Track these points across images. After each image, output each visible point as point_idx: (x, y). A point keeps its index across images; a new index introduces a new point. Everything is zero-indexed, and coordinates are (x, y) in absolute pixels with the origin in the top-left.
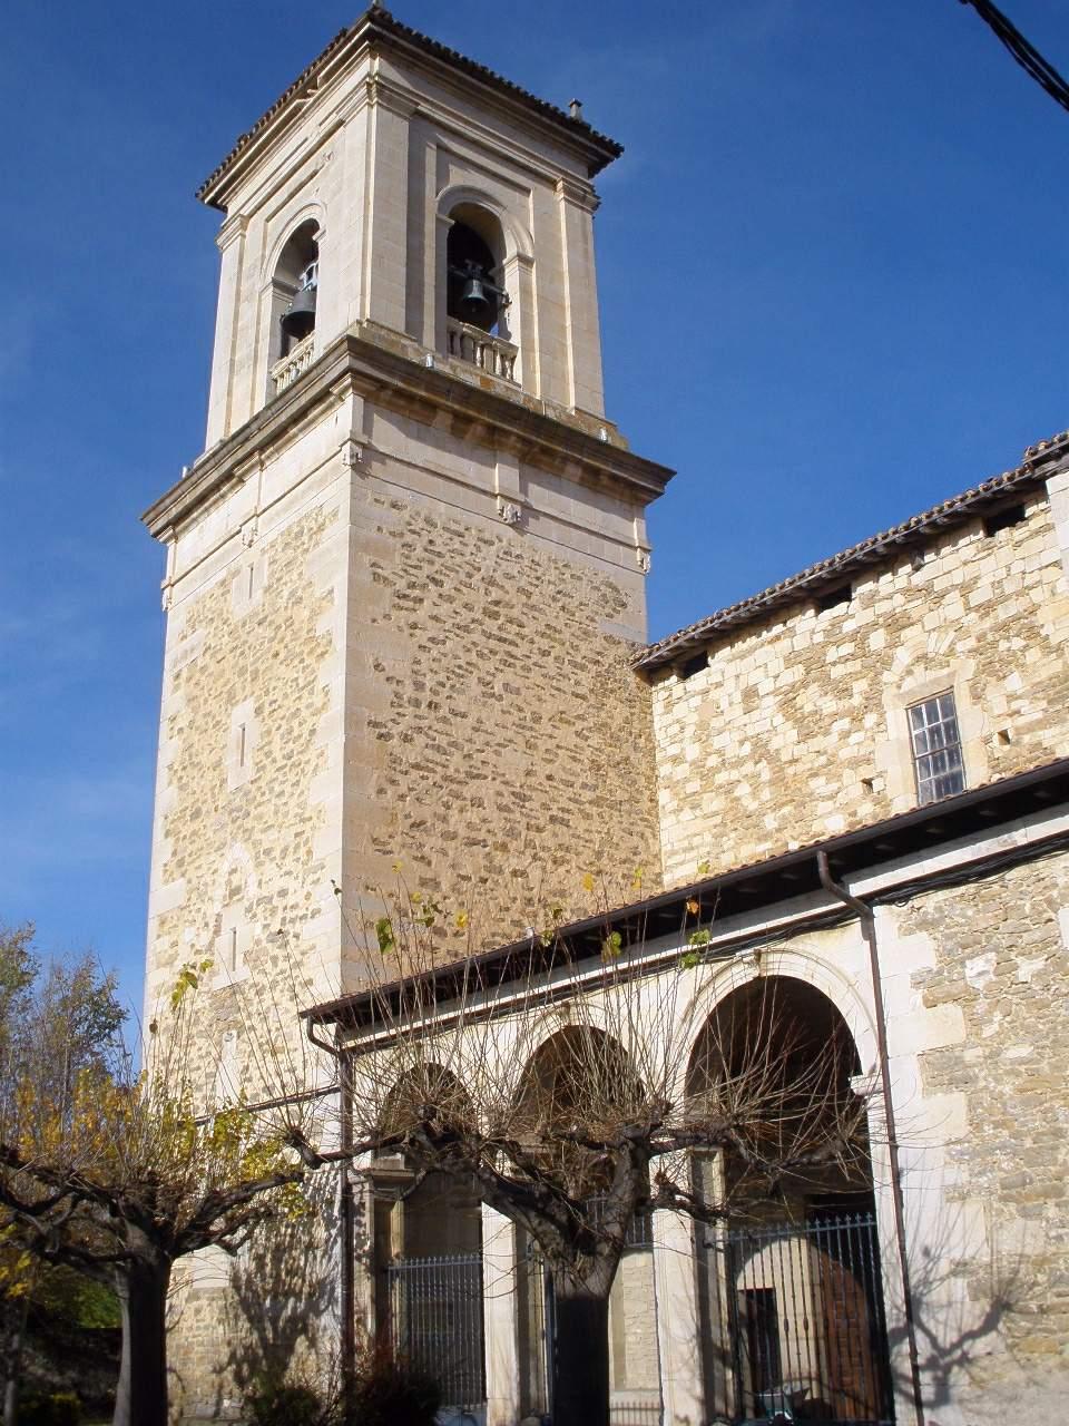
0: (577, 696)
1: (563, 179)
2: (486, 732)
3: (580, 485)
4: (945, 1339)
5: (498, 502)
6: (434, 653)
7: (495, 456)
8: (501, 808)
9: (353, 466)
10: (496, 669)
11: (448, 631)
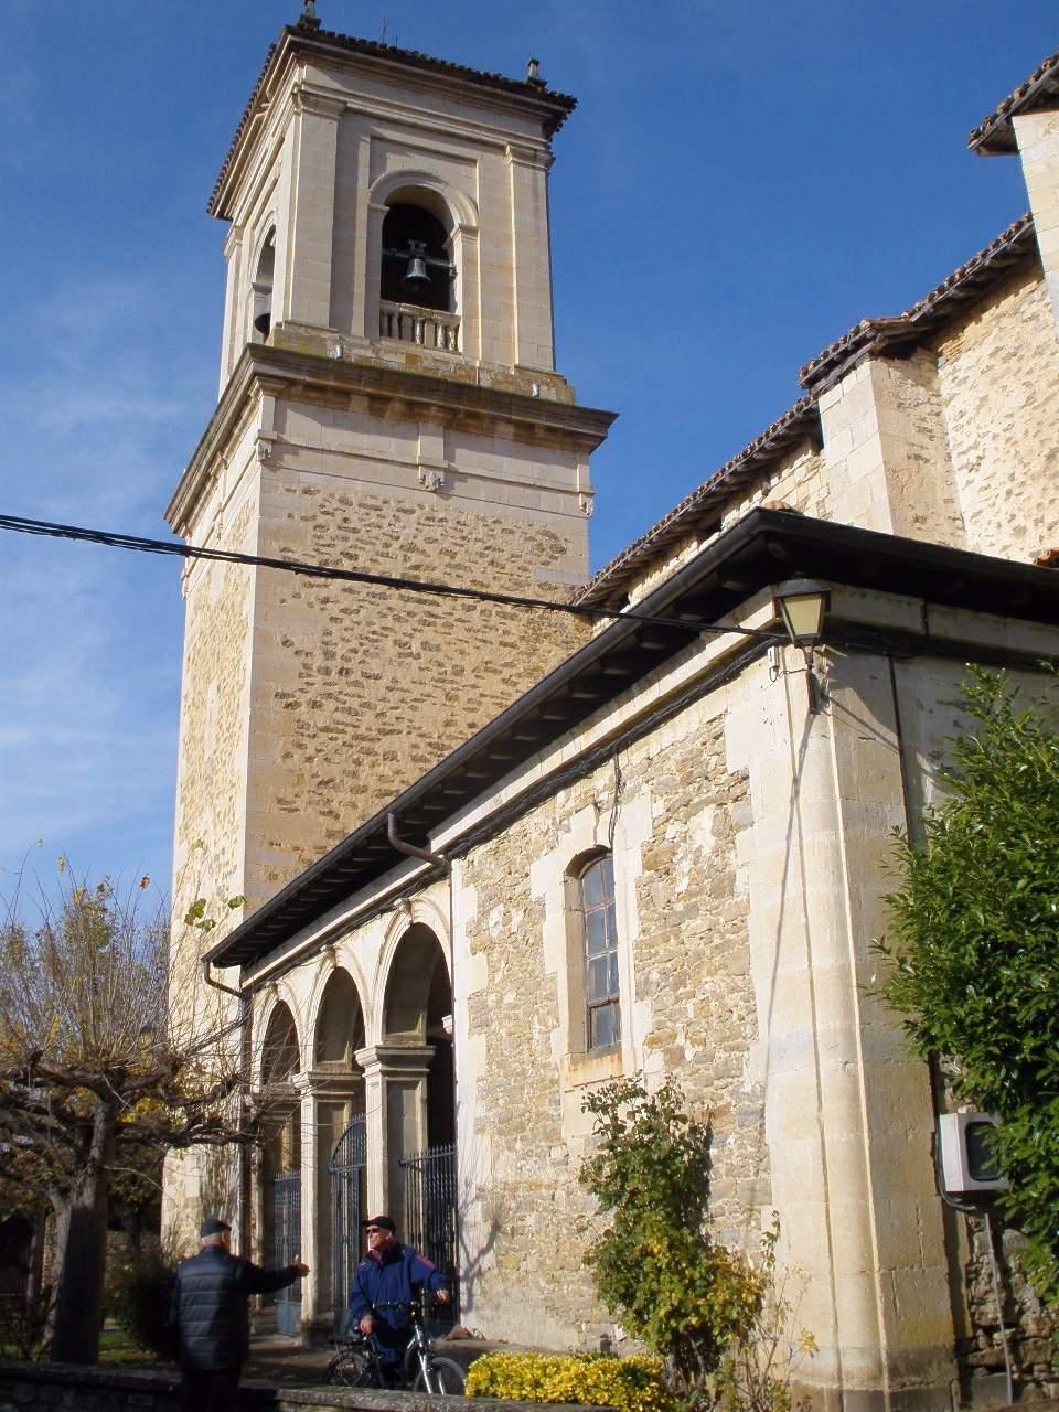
0: (505, 645)
1: (510, 143)
2: (402, 690)
3: (515, 441)
4: (215, 1274)
5: (420, 472)
6: (347, 623)
7: (418, 428)
8: (415, 759)
9: (262, 461)
10: (414, 630)
11: (362, 600)
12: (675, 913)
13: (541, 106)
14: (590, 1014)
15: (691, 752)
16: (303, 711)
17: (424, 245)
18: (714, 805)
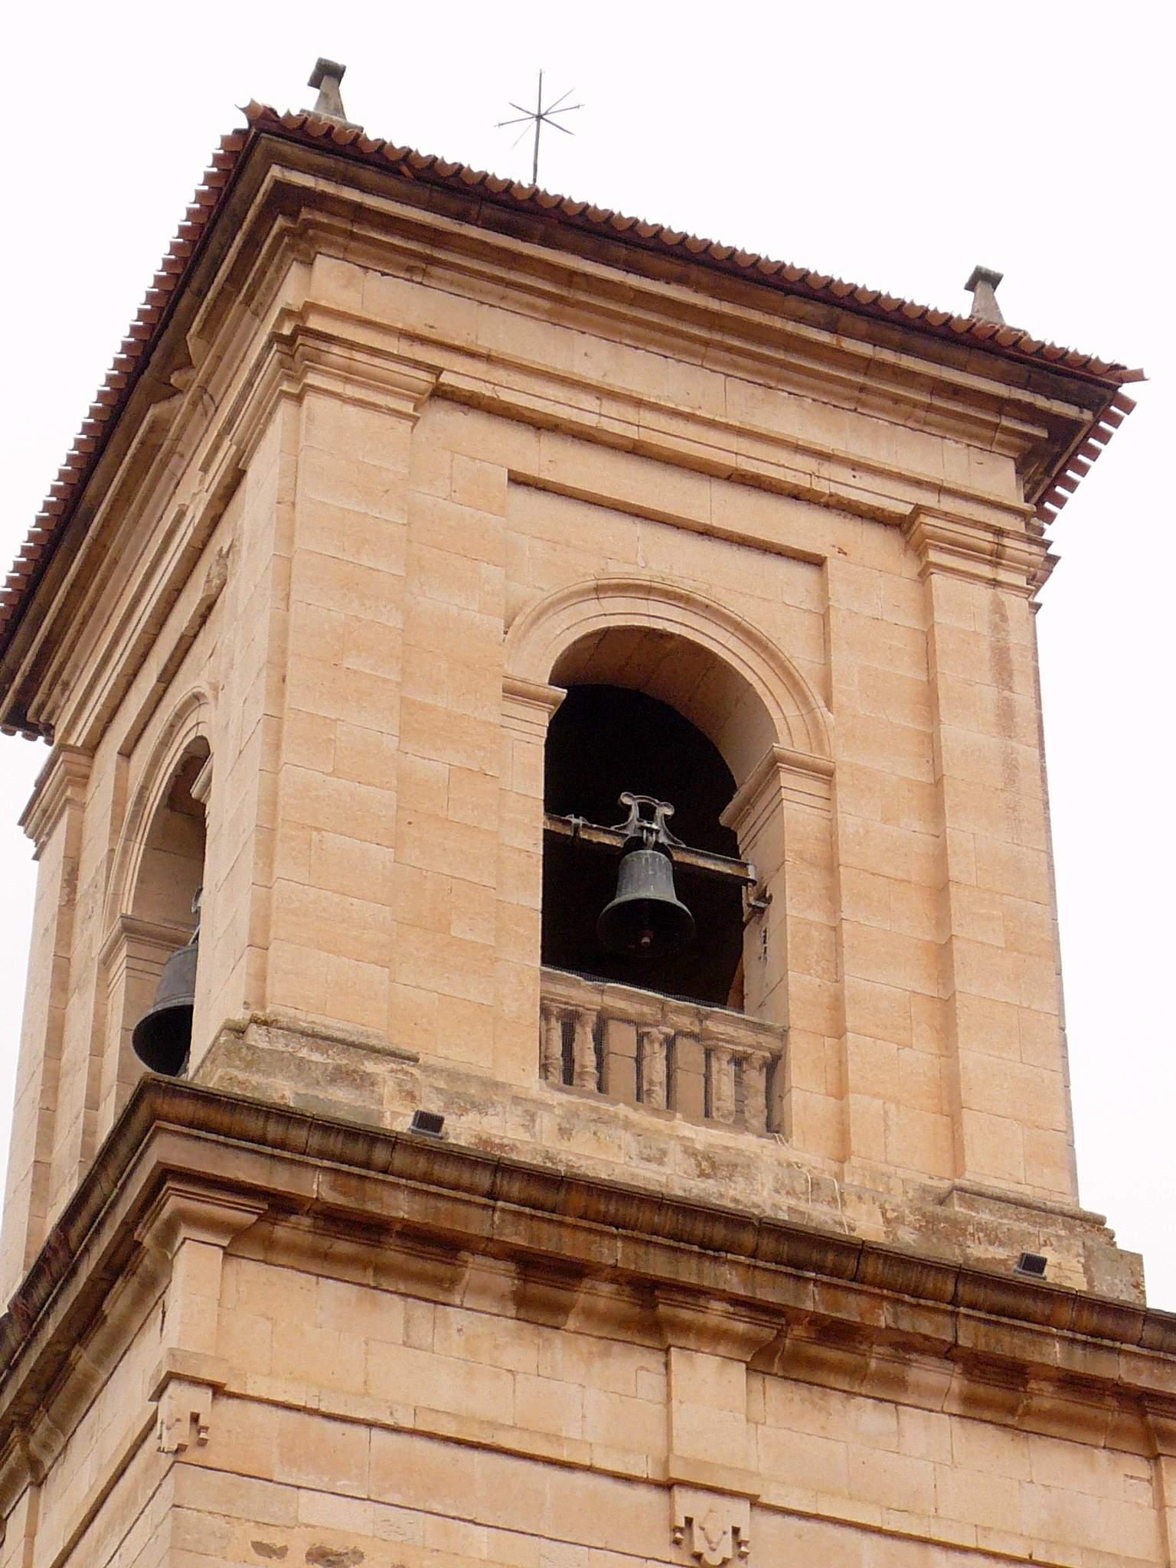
13: (1017, 403)
17: (666, 810)
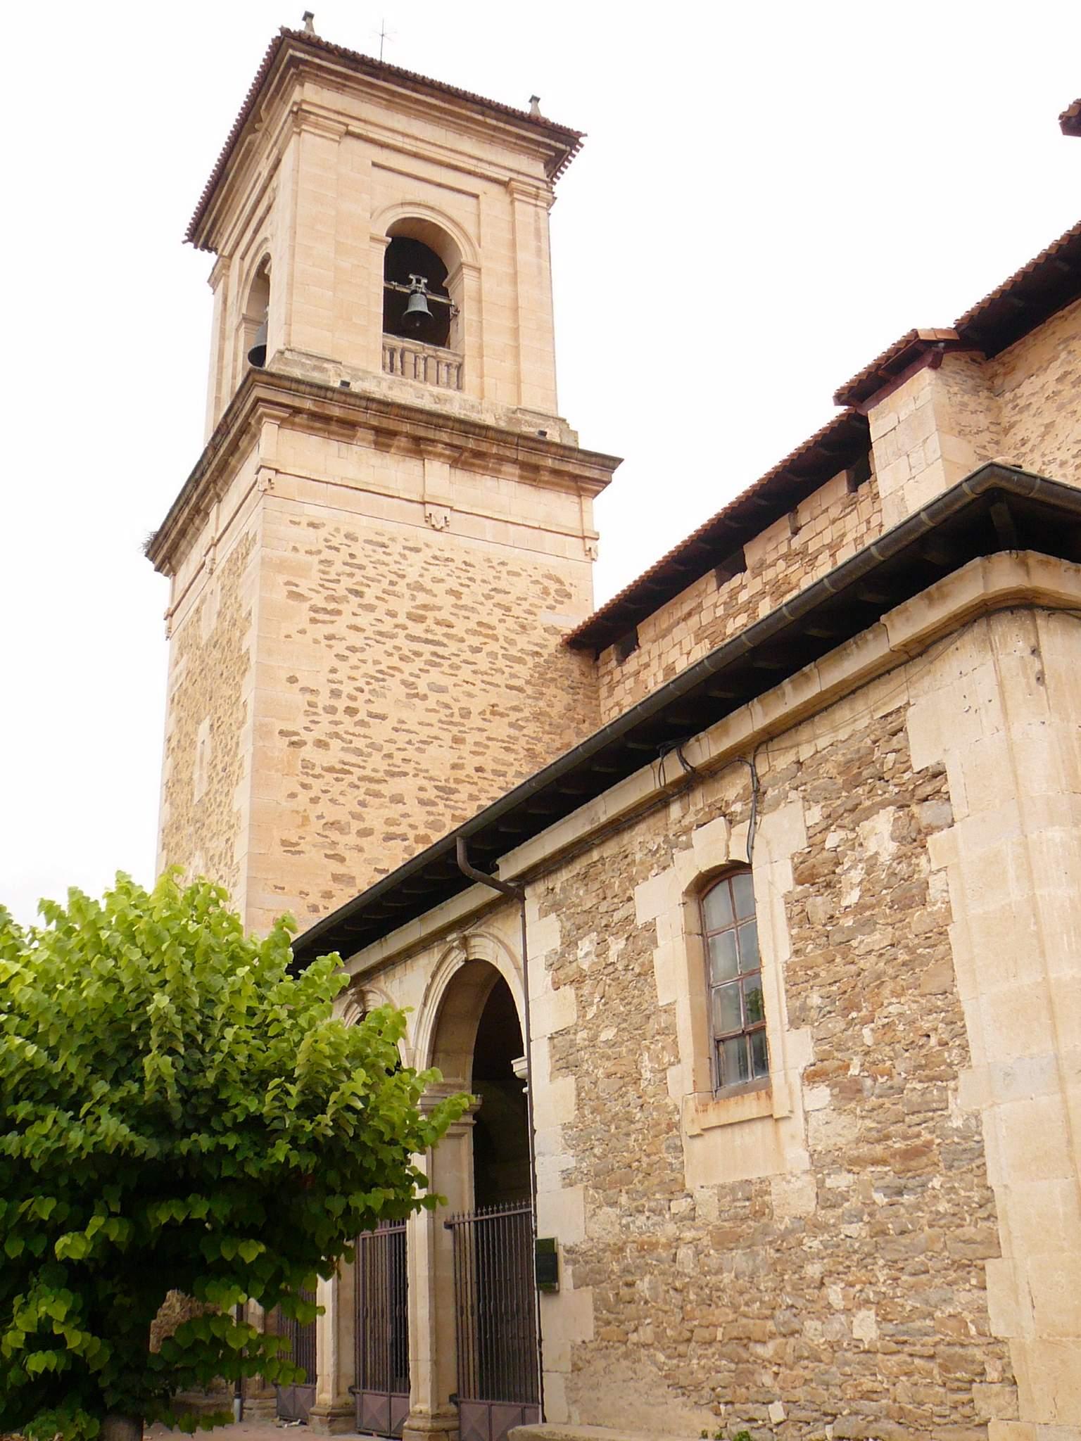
8: (422, 802)
12: (842, 930)
14: (717, 1048)
15: (858, 751)
16: (308, 752)
17: (424, 281)
18: (892, 808)
